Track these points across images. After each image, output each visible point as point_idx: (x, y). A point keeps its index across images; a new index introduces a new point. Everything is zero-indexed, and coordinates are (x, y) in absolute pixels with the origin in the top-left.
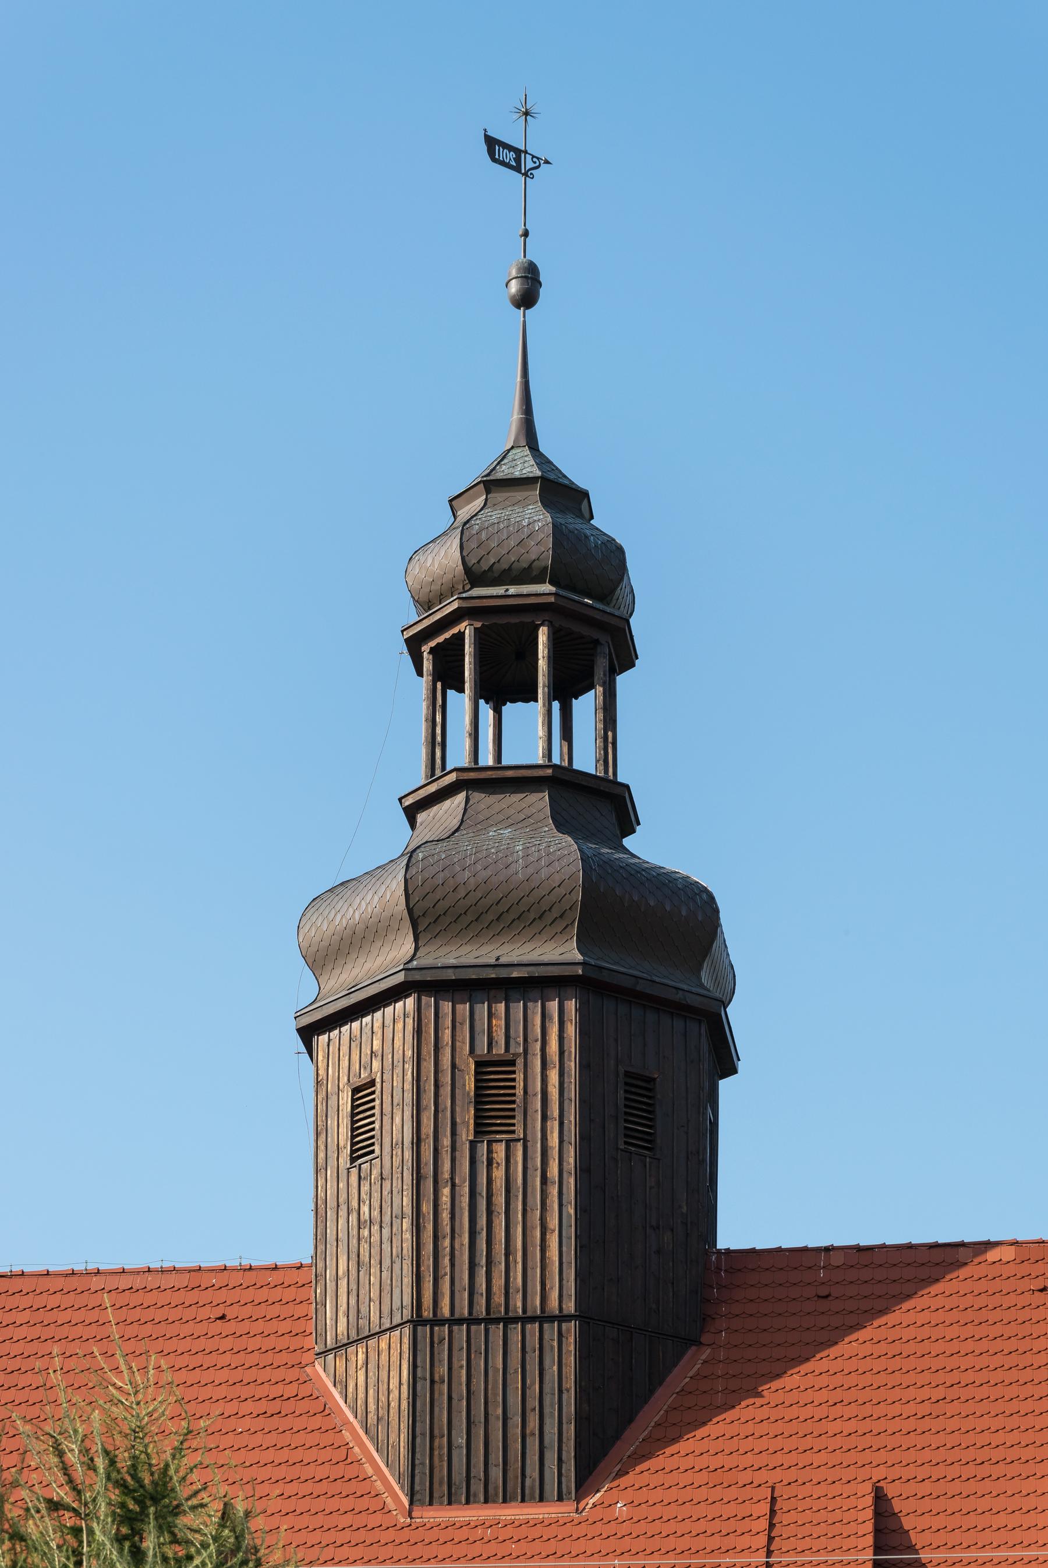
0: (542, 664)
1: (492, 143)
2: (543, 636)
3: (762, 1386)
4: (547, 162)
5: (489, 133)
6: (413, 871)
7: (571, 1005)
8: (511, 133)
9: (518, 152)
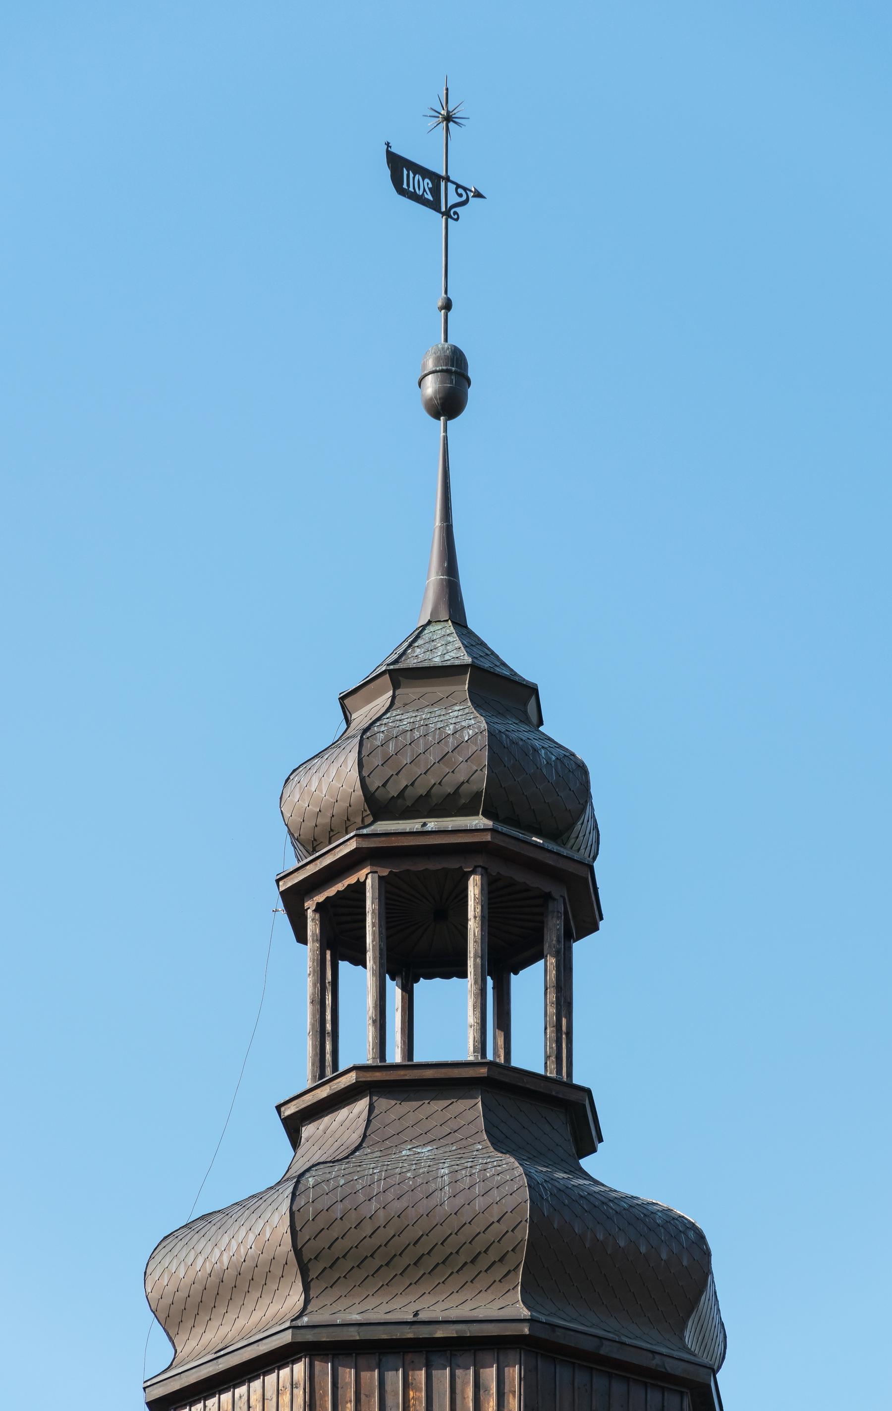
0: (474, 927)
2: (474, 888)
4: (478, 195)
5: (393, 150)
6: (301, 1201)
7: (514, 1373)
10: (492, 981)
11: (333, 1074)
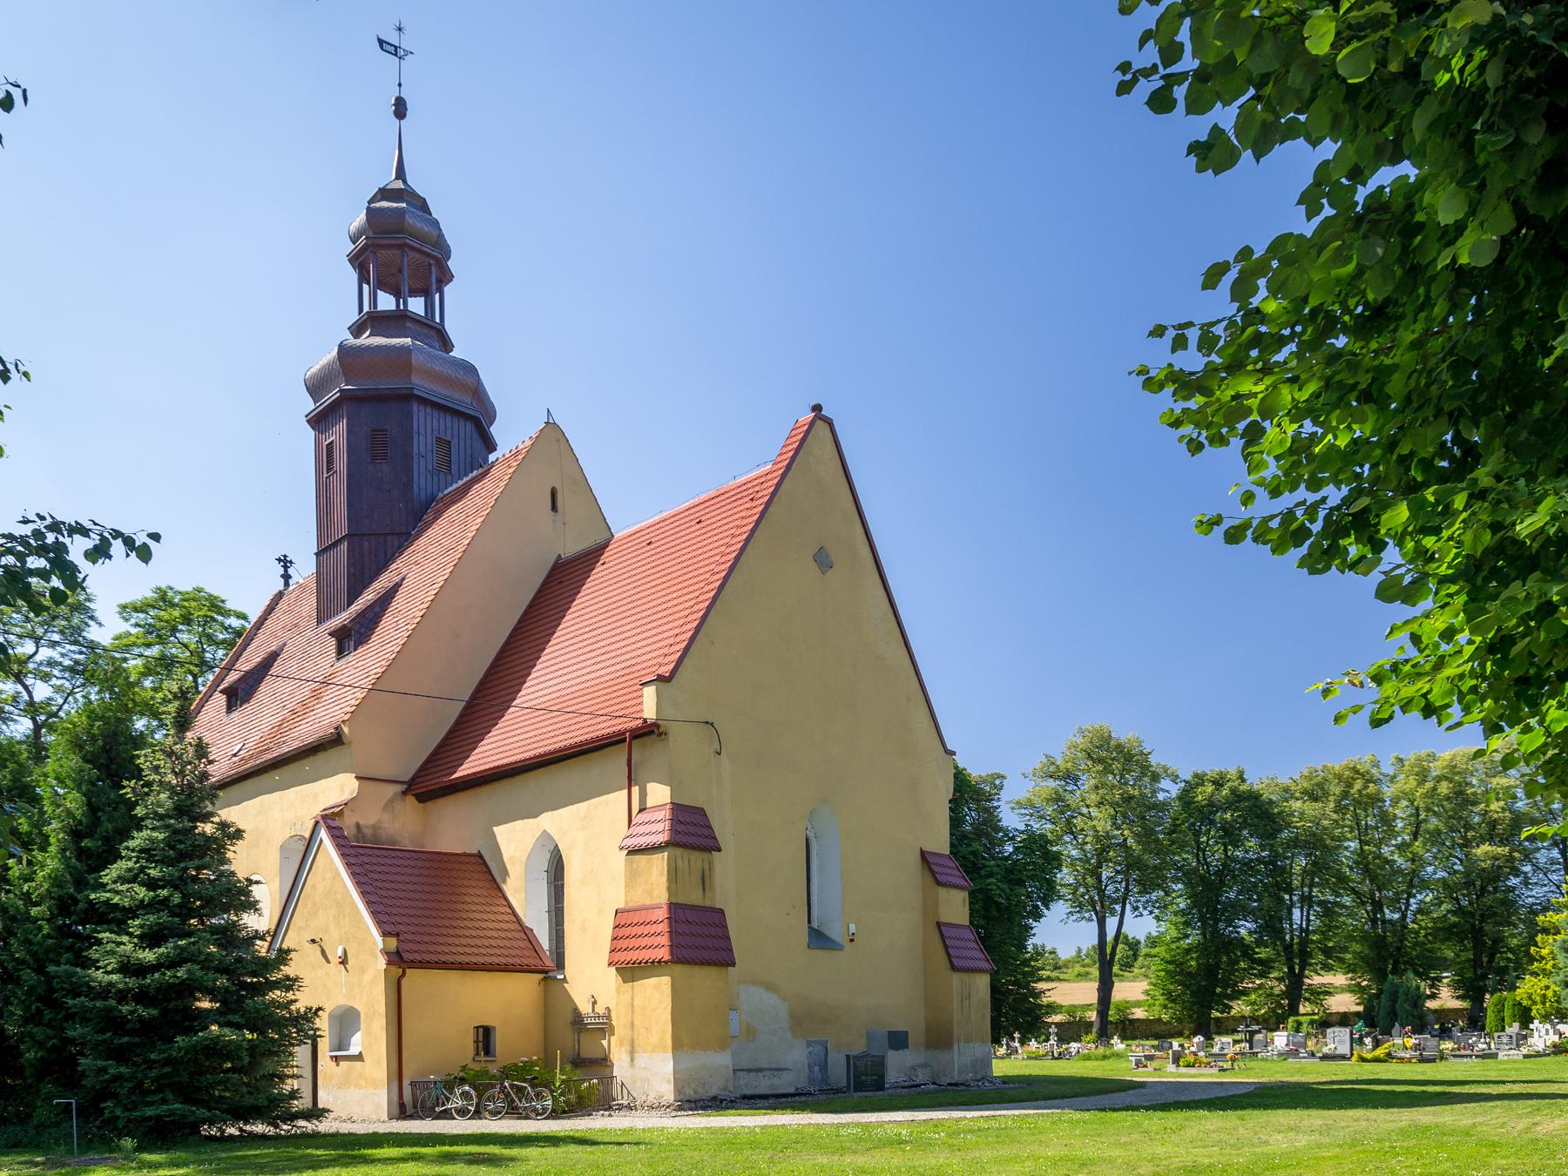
0: (395, 205)
1: (381, 42)
9: (396, 47)
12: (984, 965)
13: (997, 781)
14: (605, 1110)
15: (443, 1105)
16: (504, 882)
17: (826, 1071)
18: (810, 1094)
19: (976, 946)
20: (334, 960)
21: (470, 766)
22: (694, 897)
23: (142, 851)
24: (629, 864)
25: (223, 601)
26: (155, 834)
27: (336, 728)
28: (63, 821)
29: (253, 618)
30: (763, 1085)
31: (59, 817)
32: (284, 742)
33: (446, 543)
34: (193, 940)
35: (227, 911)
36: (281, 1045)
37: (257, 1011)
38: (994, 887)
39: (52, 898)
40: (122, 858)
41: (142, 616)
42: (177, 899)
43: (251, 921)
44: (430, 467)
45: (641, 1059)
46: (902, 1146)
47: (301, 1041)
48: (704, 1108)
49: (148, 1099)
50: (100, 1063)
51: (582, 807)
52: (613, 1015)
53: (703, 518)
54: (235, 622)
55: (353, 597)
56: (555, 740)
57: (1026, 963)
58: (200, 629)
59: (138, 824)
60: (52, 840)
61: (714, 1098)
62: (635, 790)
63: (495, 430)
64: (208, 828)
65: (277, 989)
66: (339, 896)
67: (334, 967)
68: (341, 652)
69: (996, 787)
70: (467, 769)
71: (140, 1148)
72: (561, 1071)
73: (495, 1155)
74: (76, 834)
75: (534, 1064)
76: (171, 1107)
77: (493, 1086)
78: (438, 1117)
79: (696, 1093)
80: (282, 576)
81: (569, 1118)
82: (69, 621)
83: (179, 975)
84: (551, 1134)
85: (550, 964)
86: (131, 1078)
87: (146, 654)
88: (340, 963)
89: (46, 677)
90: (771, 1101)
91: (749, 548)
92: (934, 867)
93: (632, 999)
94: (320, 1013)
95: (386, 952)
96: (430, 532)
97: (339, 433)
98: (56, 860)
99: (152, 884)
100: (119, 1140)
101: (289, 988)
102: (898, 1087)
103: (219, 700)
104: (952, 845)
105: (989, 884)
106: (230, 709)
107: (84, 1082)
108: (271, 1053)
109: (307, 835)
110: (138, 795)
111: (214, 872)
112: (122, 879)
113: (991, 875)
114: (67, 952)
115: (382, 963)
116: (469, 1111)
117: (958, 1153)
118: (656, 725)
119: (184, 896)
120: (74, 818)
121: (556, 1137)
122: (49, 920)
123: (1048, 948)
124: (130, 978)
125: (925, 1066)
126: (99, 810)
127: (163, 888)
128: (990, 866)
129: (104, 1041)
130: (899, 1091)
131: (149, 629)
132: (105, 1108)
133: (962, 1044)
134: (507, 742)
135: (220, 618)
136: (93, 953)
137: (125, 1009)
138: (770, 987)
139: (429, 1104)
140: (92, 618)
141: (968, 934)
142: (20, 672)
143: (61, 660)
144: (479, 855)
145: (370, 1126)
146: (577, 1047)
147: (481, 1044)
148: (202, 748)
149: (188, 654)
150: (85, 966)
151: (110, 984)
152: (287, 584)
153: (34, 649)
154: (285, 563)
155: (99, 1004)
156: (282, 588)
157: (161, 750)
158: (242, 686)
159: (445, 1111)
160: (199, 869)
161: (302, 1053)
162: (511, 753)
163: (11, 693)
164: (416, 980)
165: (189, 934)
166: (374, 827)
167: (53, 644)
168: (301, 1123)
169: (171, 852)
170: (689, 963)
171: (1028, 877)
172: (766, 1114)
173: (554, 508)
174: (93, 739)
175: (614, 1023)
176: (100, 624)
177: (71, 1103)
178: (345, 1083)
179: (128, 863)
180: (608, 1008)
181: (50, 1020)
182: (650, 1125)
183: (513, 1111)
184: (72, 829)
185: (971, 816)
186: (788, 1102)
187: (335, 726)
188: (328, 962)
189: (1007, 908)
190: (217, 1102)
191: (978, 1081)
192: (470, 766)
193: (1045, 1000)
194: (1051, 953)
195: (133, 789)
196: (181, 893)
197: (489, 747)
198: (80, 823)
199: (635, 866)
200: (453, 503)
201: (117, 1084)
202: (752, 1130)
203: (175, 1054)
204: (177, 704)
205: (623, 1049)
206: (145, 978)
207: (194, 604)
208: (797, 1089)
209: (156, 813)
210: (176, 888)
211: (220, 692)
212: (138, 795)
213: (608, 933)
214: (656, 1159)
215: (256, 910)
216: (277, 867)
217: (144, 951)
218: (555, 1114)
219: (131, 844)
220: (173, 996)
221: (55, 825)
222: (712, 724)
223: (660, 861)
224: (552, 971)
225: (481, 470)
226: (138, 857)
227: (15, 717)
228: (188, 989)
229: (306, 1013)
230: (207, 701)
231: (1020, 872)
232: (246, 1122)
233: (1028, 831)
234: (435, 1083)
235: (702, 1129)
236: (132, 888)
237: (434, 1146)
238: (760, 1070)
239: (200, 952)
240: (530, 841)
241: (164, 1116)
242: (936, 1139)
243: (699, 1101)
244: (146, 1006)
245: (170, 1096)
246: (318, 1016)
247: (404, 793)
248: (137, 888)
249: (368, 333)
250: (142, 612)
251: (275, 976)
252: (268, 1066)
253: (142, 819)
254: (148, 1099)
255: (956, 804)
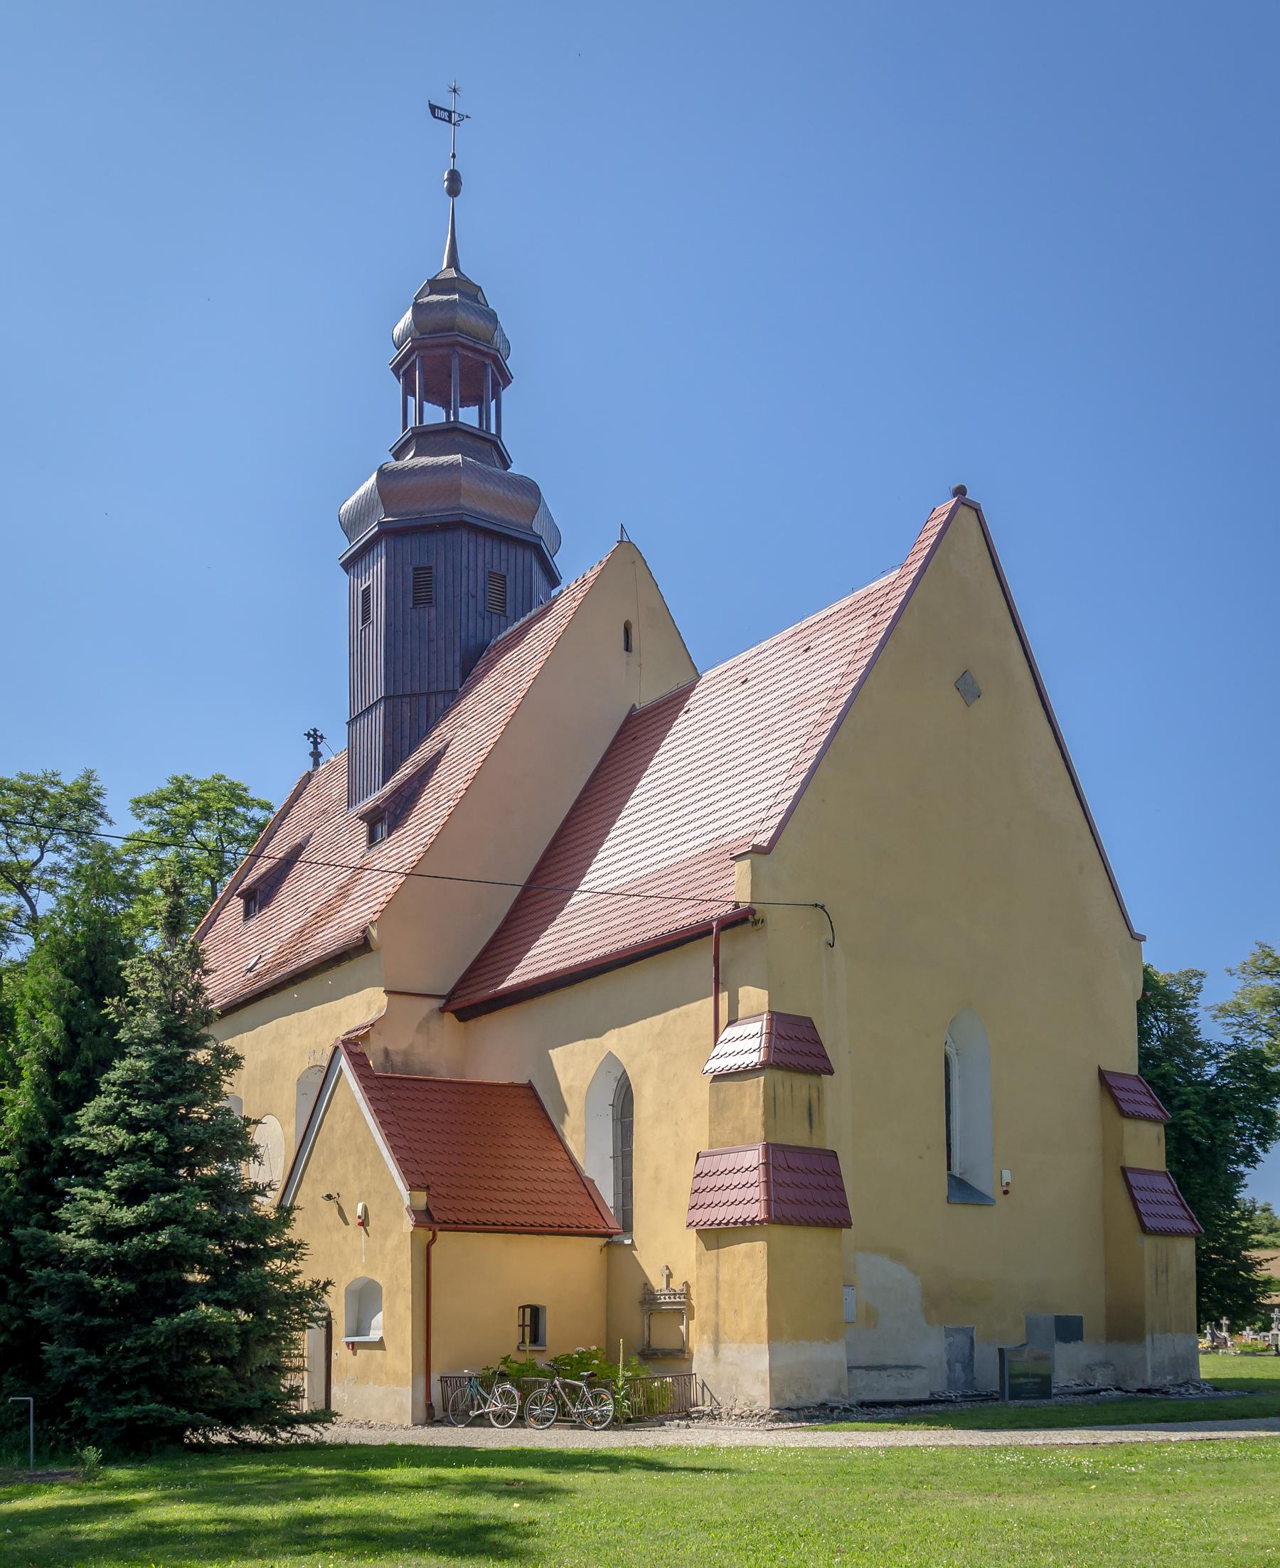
0: (445, 298)
1: (433, 108)
3: (438, 301)
4: (467, 117)
5: (432, 103)
8: (447, 102)
9: (450, 113)
10: (400, 1444)
11: (1009, 1384)
12: (1186, 1226)
13: (1194, 980)
14: (681, 1419)
15: (479, 1408)
16: (562, 1121)
17: (972, 1367)
18: (951, 1401)
19: (1176, 1200)
20: (354, 1221)
21: (521, 974)
22: (797, 1135)
23: (125, 1084)
24: (714, 1093)
25: (245, 790)
26: (139, 1063)
27: (363, 932)
28: (38, 1049)
29: (277, 810)
30: (887, 1388)
31: (34, 1046)
32: (305, 952)
33: (497, 699)
34: (178, 1195)
35: (220, 1159)
36: (278, 1330)
37: (252, 1286)
38: (1191, 1121)
39: (22, 1145)
40: (100, 1093)
41: (156, 811)
42: (162, 1144)
43: (251, 1172)
44: (480, 608)
45: (728, 1351)
46: (1086, 1483)
47: (304, 1324)
48: (809, 1419)
49: (119, 1397)
50: (67, 1351)
51: (657, 1020)
52: (693, 1292)
53: (812, 645)
54: (257, 814)
55: (389, 769)
56: (624, 935)
57: (1233, 1223)
58: (221, 825)
59: (120, 1051)
60: (25, 1073)
61: (823, 1406)
62: (724, 997)
63: (560, 562)
64: (202, 1055)
65: (277, 1257)
66: (360, 1140)
67: (353, 1230)
68: (372, 840)
69: (1192, 989)
70: (518, 976)
71: (106, 1461)
72: (624, 1365)
73: (533, 1483)
74: (52, 1065)
75: (592, 1355)
76: (146, 1407)
77: (541, 1385)
78: (472, 1424)
79: (798, 1398)
80: (312, 754)
81: (634, 1429)
82: (77, 820)
83: (160, 1239)
84: (609, 1453)
85: (614, 1224)
86: (103, 1369)
87: (160, 856)
88: (361, 1224)
89: (50, 888)
90: (897, 1410)
91: (871, 677)
92: (1117, 1092)
93: (717, 1271)
94: (329, 1288)
95: (414, 1212)
96: (479, 687)
97: (376, 574)
98: (28, 1098)
99: (134, 1126)
100: (82, 1449)
101: (290, 1256)
102: (1069, 1394)
103: (237, 904)
104: (1140, 1069)
105: (1184, 1118)
106: (248, 914)
107: (50, 1374)
108: (266, 1339)
109: (325, 1064)
110: (122, 1015)
111: (206, 1110)
112: (98, 1120)
113: (1186, 1105)
114: (37, 1211)
115: (408, 1223)
116: (510, 1417)
117: (1166, 1497)
118: (751, 911)
119: (171, 1140)
120: (51, 1046)
121: (616, 1458)
122: (17, 1173)
123: (1260, 1204)
124: (105, 1243)
125: (1106, 1364)
126: (79, 1035)
127: (146, 1130)
128: (1185, 1094)
129: (73, 1323)
130: (1071, 1398)
131: (164, 826)
132: (72, 1408)
133: (1157, 1335)
134: (566, 940)
135: (241, 810)
136: (64, 1213)
137: (98, 1282)
138: (897, 1256)
139: (462, 1407)
140: (101, 815)
141: (1164, 1184)
142: (24, 882)
143: (66, 865)
144: (530, 1087)
145: (390, 1434)
146: (647, 1334)
147: (527, 1330)
148: (197, 955)
149: (206, 854)
150: (55, 1229)
151: (82, 1251)
152: (316, 764)
153: (39, 855)
154: (315, 739)
155: (68, 1276)
156: (311, 769)
157: (149, 958)
158: (262, 888)
159: (481, 1416)
160: (189, 1106)
161: (309, 1341)
162: (571, 954)
163: (12, 907)
164: (448, 1242)
165: (175, 1189)
166: (405, 1053)
167: (59, 849)
168: (304, 1429)
169: (157, 1085)
170: (791, 1224)
171: (1238, 1108)
172: (891, 1429)
173: (628, 648)
174: (77, 948)
175: (694, 1302)
176: (111, 822)
177: (29, 1401)
178: (362, 1377)
179: (108, 1099)
180: (686, 1283)
181: (16, 1296)
182: (738, 1442)
183: (564, 1418)
184: (48, 1060)
185: (1160, 1027)
186: (920, 1412)
187: (362, 928)
188: (347, 1223)
189: (1209, 1149)
190: (202, 1402)
191: (1180, 1386)
192: (521, 974)
193: (1261, 1274)
194: (1264, 1210)
195: (117, 1008)
196: (167, 1136)
197: (544, 948)
198: (57, 1050)
199: (722, 1095)
200: (508, 649)
201: (86, 1377)
202: (872, 1453)
203: (153, 1341)
204: (168, 901)
205: (705, 1337)
206: (121, 1244)
207: (213, 795)
208: (932, 1394)
209: (141, 1037)
210: (161, 1129)
211: (238, 896)
212: (122, 1015)
213: (688, 1184)
214: (744, 1494)
215: (256, 1157)
216: (293, 1104)
217: (121, 1209)
218: (619, 1422)
219: (112, 1075)
220: (154, 1266)
221: (31, 1054)
222: (822, 907)
223: (755, 1089)
224: (618, 1234)
225: (541, 608)
226: (119, 1093)
227: (16, 935)
228: (174, 1258)
229: (311, 1289)
230: (224, 908)
231: (1227, 1101)
232: (238, 1428)
233: (1237, 1045)
234: (470, 1379)
235: (806, 1449)
236: (110, 1130)
237: (459, 1466)
238: (883, 1368)
239: (186, 1211)
240: (592, 1066)
241: (138, 1419)
242: (1131, 1474)
243: (802, 1409)
244: (122, 1280)
245: (145, 1393)
246: (327, 1293)
247: (442, 1010)
248: (115, 1130)
249: (412, 453)
250: (157, 807)
251: (272, 1241)
252: (264, 1356)
253: (126, 1045)
254: (119, 1397)
255: (1144, 1008)
